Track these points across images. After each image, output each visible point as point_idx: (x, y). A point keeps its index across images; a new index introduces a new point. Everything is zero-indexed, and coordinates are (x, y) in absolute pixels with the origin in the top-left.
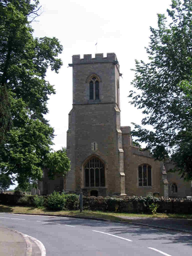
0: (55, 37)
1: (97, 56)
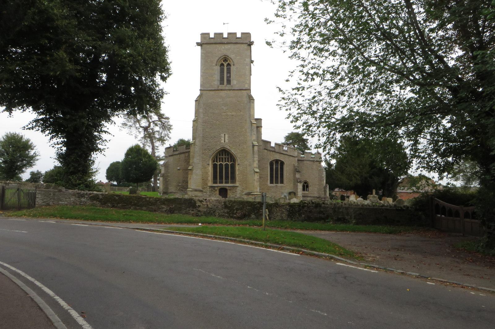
0: (275, 14)
1: (243, 35)
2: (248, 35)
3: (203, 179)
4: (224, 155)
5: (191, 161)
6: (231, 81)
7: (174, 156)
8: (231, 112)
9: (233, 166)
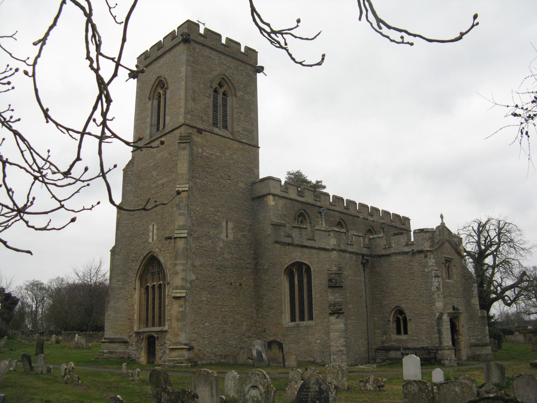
2: (218, 36)
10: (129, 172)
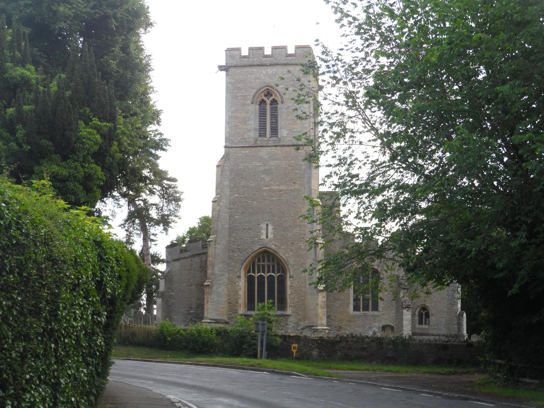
3: (230, 303)
4: (266, 260)
5: (209, 271)
6: (279, 130)
7: (182, 261)
8: (278, 185)
9: (282, 281)
10: (226, 168)
